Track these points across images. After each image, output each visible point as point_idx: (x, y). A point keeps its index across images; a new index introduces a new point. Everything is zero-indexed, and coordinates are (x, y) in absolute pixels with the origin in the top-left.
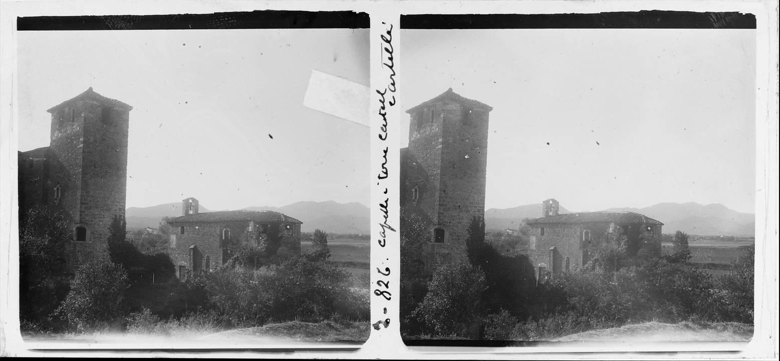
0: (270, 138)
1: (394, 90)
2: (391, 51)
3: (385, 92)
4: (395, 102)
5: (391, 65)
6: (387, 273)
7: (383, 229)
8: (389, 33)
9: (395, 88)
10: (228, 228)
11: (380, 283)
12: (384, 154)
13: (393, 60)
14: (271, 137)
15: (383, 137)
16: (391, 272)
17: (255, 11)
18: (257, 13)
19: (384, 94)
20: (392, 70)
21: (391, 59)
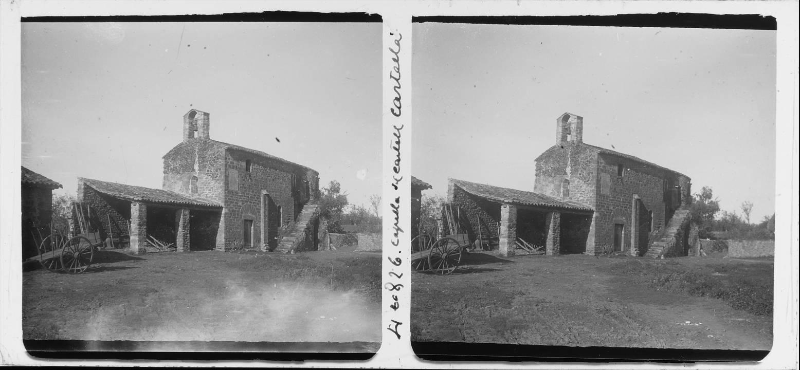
0: (276, 141)
1: (398, 113)
2: (398, 135)
3: (399, 51)
4: (398, 58)
5: (398, 78)
6: (398, 263)
7: (396, 330)
8: (397, 201)
9: (400, 103)
10: (631, 198)
11: (392, 274)
12: (396, 222)
13: (400, 145)
14: (278, 140)
15: (396, 243)
16: (401, 265)
17: (659, 14)
18: (661, 15)
19: (398, 53)
20: (398, 82)
21: (398, 143)
